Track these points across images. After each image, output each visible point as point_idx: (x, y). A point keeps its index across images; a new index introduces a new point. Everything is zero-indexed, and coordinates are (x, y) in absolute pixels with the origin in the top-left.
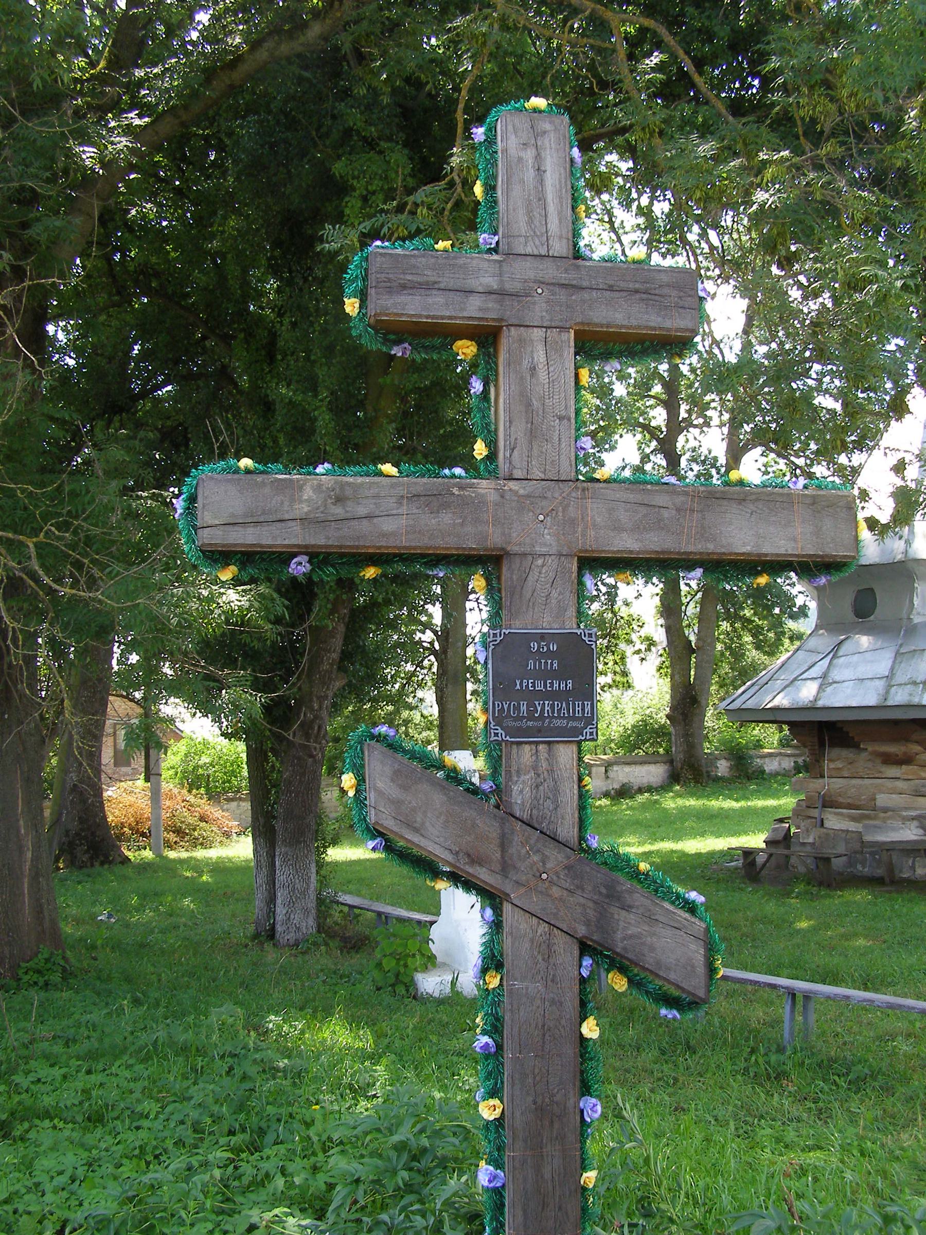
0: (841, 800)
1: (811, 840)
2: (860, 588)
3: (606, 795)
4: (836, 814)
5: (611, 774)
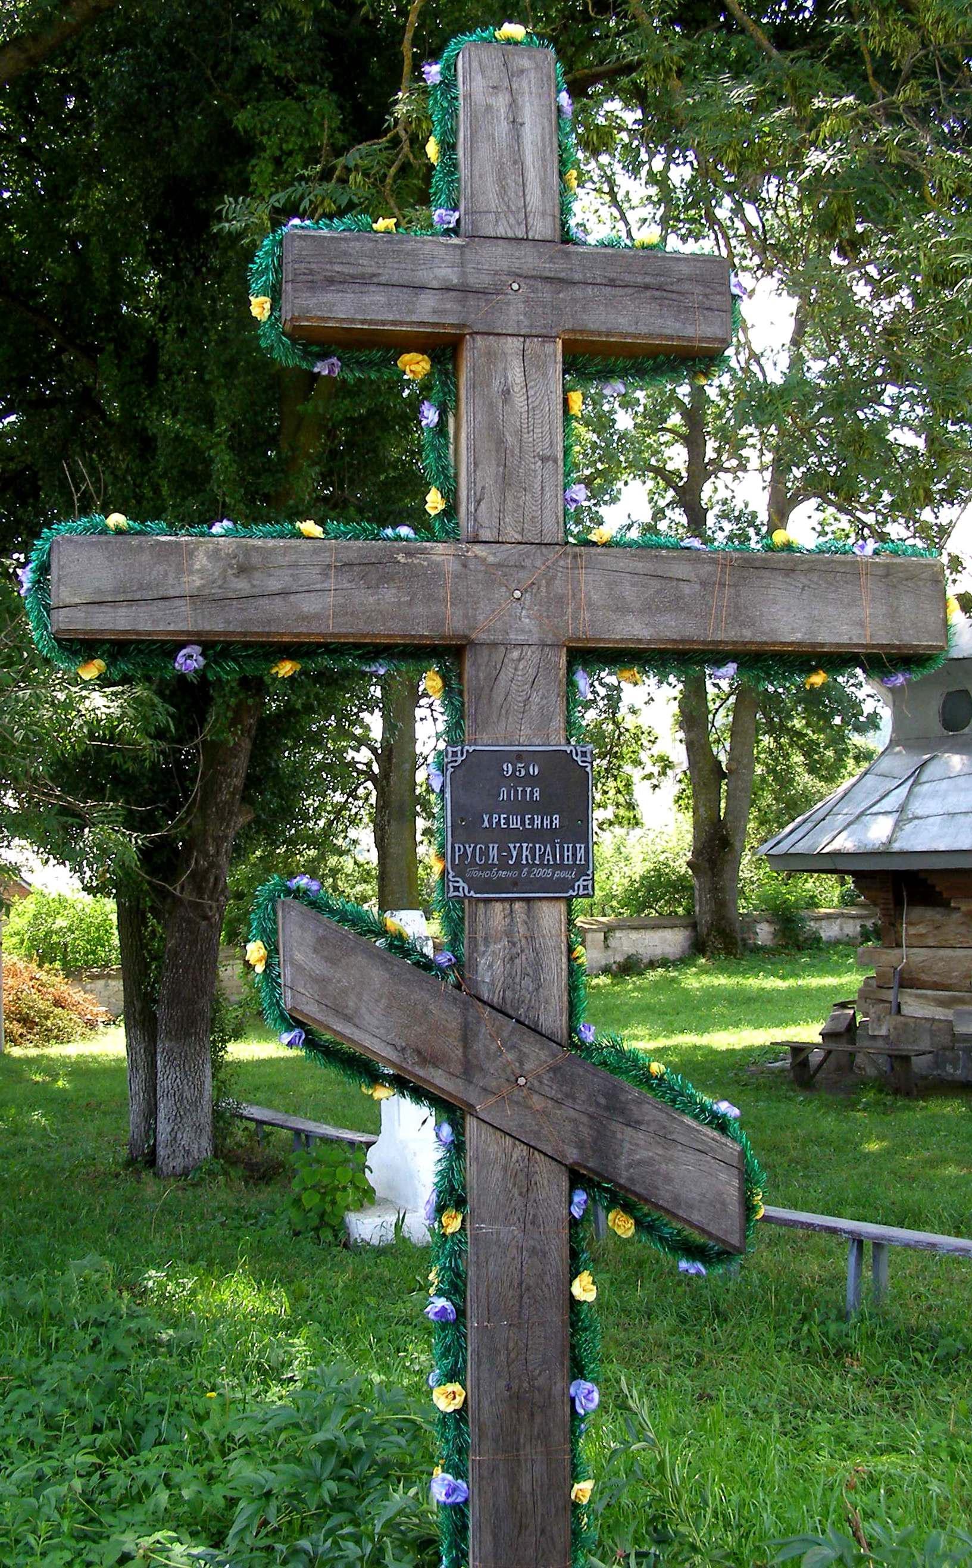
0: (924, 977)
1: (883, 1032)
2: (951, 690)
3: (606, 970)
4: (917, 996)
5: (612, 943)
